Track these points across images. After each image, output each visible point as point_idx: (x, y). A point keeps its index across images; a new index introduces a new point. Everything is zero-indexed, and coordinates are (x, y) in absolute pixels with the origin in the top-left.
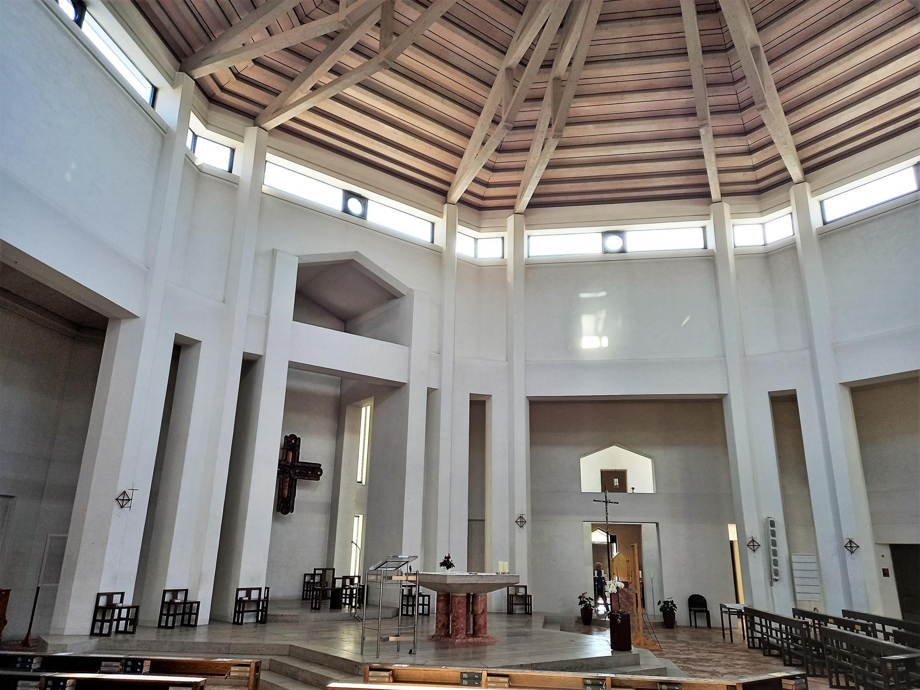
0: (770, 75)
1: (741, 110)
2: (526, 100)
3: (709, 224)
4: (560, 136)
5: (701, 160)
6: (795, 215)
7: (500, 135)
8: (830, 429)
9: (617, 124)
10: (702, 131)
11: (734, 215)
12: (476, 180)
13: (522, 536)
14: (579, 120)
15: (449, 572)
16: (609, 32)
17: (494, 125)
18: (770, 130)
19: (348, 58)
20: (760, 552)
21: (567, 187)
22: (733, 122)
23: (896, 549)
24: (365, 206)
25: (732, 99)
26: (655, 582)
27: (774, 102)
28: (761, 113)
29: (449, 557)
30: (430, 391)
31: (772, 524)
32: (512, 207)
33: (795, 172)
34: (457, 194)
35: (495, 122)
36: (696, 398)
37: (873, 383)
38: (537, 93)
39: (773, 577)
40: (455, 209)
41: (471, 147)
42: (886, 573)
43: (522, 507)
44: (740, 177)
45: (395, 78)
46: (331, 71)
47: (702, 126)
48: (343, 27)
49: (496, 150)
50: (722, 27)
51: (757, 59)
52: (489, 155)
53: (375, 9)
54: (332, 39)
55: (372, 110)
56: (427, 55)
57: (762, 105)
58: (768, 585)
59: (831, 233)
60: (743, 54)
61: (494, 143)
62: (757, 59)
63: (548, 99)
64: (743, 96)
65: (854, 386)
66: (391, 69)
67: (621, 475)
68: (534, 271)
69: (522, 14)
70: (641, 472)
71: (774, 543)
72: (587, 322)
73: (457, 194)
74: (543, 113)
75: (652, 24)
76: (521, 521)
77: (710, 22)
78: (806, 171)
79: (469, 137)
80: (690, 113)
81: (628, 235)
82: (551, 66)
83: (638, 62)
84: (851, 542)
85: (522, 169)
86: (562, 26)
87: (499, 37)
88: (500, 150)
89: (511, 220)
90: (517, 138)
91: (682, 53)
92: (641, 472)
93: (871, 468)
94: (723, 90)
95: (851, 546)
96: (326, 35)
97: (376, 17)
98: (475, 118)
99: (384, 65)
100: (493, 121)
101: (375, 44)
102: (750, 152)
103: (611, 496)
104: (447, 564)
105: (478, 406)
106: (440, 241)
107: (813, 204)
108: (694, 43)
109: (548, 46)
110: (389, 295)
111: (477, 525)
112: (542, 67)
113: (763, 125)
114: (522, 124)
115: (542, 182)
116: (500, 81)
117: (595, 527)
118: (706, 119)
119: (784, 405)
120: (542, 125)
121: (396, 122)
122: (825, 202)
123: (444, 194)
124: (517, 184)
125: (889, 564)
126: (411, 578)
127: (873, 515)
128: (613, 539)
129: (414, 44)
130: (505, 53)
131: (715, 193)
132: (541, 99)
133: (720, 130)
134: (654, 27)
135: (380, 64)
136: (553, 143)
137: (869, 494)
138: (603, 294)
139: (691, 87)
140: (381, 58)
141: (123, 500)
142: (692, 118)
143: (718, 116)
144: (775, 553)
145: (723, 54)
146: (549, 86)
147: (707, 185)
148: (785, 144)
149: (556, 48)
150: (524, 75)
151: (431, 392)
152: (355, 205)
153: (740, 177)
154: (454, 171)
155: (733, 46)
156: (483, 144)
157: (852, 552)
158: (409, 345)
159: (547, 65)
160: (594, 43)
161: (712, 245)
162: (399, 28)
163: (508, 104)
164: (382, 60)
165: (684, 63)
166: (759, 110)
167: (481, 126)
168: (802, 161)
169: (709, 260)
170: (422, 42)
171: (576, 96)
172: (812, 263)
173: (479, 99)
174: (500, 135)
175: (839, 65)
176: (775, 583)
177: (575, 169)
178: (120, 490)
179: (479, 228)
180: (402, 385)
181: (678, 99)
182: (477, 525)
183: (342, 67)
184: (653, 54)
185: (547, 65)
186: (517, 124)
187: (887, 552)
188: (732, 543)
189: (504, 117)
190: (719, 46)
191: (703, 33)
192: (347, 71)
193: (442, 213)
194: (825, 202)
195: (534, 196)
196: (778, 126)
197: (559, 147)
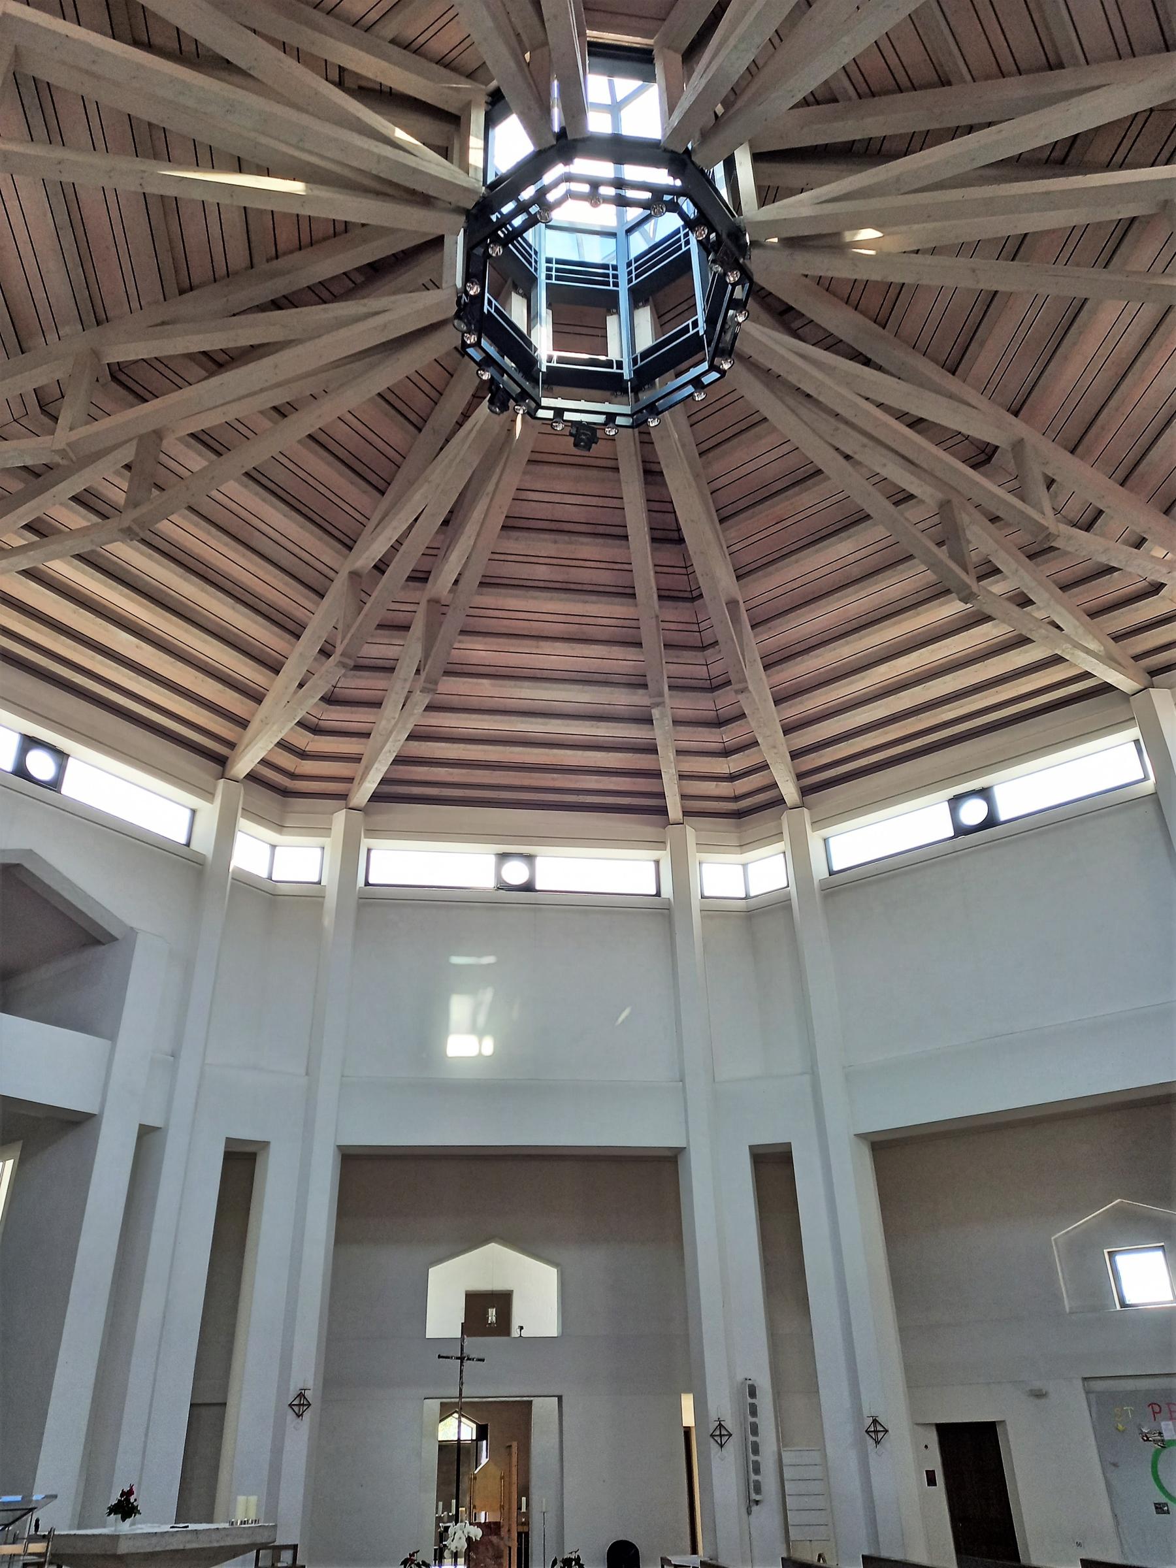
0: (753, 645)
1: (713, 689)
2: (381, 626)
3: (665, 856)
4: (434, 691)
5: (654, 756)
6: (789, 854)
7: (329, 675)
8: (840, 1210)
9: (526, 684)
10: (656, 713)
11: (702, 846)
12: (282, 745)
13: (299, 1436)
14: (467, 669)
15: (126, 1527)
16: (518, 544)
17: (324, 659)
18: (753, 724)
19: (64, 511)
20: (732, 1446)
21: (441, 774)
22: (702, 705)
23: (945, 1431)
24: (61, 769)
25: (702, 672)
26: (551, 1518)
27: (759, 687)
28: (740, 697)
29: (131, 1492)
30: (145, 1132)
31: (753, 1393)
32: (344, 797)
33: (789, 790)
34: (244, 764)
35: (325, 653)
36: (596, 1152)
37: (897, 1136)
38: (401, 618)
39: (752, 1498)
40: (240, 789)
41: (280, 686)
42: (931, 1479)
43: (305, 1374)
44: (710, 788)
45: (150, 557)
46: (28, 527)
47: (657, 705)
48: (57, 459)
49: (322, 699)
50: (687, 567)
51: (736, 620)
52: (309, 705)
53: (126, 442)
54: (38, 475)
55: (99, 603)
56: (213, 530)
57: (740, 686)
58: (744, 1510)
59: (847, 888)
60: (714, 609)
61: (319, 687)
62: (736, 620)
63: (418, 628)
64: (716, 670)
65: (877, 1138)
66: (143, 541)
67: (503, 1301)
68: (377, 906)
69: (383, 493)
70: (538, 1294)
71: (755, 1430)
72: (460, 1008)
73: (244, 764)
74: (408, 651)
75: (587, 544)
76: (300, 1404)
77: (669, 555)
78: (805, 792)
79: (277, 672)
80: (638, 683)
81: (539, 861)
82: (425, 580)
83: (563, 595)
84: (875, 1422)
85: (367, 735)
86: (446, 523)
87: (343, 522)
88: (330, 700)
89: (340, 819)
90: (362, 683)
91: (629, 594)
92: (538, 1294)
93: (907, 1285)
94: (688, 656)
95: (876, 1431)
96: (25, 468)
97: (127, 454)
98: (289, 642)
99: (129, 534)
100: (321, 651)
101: (118, 497)
102: (726, 753)
103: (475, 1345)
104: (125, 1508)
105: (241, 1164)
106: (204, 844)
107: (814, 840)
108: (646, 581)
109: (422, 549)
110: (89, 934)
111: (207, 1415)
112: (410, 579)
113: (743, 716)
114: (366, 662)
115: (399, 761)
116: (338, 588)
117: (446, 1411)
118: (661, 695)
119: (773, 1167)
120: (406, 669)
121: (144, 628)
122: (831, 841)
123: (221, 761)
124: (357, 759)
125: (935, 1462)
126: (37, 1547)
127: (908, 1368)
128: (482, 1432)
129: (191, 509)
130: (350, 549)
131: (674, 809)
132: (406, 628)
133: (682, 714)
134: (589, 549)
135: (121, 530)
136: (421, 700)
137: (902, 1330)
138: (489, 960)
139: (640, 645)
140: (127, 520)
141: (299, 1405)
142: (641, 691)
143: (680, 694)
144: (756, 1450)
145: (688, 605)
146: (421, 610)
147: (662, 795)
148: (774, 747)
149: (436, 552)
150: (380, 585)
151: (147, 1135)
152: (40, 765)
153: (710, 788)
154: (243, 724)
155: (701, 596)
156: (301, 686)
157: (877, 1442)
158: (112, 1037)
159: (420, 577)
160: (496, 556)
161: (667, 891)
162: (162, 476)
163: (349, 627)
164: (126, 524)
165: (632, 609)
166: (738, 692)
167: (300, 656)
168: (800, 776)
169: (661, 914)
170: (207, 507)
171: (463, 632)
172: (813, 928)
173: (299, 613)
174: (329, 675)
175: (847, 643)
176: (755, 1508)
177: (456, 746)
178: (293, 1393)
179: (280, 827)
180: (89, 1117)
181: (622, 660)
182: (207, 1415)
183: (50, 525)
184: (585, 587)
185: (420, 577)
186: (362, 662)
187: (933, 1438)
188: (687, 1431)
189: (339, 649)
190: (681, 592)
191: (659, 569)
192: (60, 532)
193: (213, 794)
194: (831, 840)
195: (383, 781)
196: (765, 721)
197: (430, 708)
